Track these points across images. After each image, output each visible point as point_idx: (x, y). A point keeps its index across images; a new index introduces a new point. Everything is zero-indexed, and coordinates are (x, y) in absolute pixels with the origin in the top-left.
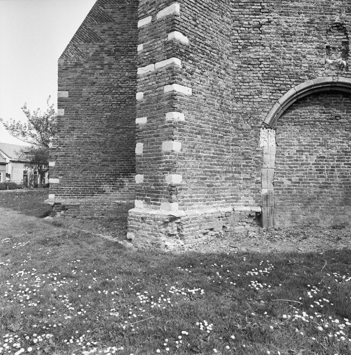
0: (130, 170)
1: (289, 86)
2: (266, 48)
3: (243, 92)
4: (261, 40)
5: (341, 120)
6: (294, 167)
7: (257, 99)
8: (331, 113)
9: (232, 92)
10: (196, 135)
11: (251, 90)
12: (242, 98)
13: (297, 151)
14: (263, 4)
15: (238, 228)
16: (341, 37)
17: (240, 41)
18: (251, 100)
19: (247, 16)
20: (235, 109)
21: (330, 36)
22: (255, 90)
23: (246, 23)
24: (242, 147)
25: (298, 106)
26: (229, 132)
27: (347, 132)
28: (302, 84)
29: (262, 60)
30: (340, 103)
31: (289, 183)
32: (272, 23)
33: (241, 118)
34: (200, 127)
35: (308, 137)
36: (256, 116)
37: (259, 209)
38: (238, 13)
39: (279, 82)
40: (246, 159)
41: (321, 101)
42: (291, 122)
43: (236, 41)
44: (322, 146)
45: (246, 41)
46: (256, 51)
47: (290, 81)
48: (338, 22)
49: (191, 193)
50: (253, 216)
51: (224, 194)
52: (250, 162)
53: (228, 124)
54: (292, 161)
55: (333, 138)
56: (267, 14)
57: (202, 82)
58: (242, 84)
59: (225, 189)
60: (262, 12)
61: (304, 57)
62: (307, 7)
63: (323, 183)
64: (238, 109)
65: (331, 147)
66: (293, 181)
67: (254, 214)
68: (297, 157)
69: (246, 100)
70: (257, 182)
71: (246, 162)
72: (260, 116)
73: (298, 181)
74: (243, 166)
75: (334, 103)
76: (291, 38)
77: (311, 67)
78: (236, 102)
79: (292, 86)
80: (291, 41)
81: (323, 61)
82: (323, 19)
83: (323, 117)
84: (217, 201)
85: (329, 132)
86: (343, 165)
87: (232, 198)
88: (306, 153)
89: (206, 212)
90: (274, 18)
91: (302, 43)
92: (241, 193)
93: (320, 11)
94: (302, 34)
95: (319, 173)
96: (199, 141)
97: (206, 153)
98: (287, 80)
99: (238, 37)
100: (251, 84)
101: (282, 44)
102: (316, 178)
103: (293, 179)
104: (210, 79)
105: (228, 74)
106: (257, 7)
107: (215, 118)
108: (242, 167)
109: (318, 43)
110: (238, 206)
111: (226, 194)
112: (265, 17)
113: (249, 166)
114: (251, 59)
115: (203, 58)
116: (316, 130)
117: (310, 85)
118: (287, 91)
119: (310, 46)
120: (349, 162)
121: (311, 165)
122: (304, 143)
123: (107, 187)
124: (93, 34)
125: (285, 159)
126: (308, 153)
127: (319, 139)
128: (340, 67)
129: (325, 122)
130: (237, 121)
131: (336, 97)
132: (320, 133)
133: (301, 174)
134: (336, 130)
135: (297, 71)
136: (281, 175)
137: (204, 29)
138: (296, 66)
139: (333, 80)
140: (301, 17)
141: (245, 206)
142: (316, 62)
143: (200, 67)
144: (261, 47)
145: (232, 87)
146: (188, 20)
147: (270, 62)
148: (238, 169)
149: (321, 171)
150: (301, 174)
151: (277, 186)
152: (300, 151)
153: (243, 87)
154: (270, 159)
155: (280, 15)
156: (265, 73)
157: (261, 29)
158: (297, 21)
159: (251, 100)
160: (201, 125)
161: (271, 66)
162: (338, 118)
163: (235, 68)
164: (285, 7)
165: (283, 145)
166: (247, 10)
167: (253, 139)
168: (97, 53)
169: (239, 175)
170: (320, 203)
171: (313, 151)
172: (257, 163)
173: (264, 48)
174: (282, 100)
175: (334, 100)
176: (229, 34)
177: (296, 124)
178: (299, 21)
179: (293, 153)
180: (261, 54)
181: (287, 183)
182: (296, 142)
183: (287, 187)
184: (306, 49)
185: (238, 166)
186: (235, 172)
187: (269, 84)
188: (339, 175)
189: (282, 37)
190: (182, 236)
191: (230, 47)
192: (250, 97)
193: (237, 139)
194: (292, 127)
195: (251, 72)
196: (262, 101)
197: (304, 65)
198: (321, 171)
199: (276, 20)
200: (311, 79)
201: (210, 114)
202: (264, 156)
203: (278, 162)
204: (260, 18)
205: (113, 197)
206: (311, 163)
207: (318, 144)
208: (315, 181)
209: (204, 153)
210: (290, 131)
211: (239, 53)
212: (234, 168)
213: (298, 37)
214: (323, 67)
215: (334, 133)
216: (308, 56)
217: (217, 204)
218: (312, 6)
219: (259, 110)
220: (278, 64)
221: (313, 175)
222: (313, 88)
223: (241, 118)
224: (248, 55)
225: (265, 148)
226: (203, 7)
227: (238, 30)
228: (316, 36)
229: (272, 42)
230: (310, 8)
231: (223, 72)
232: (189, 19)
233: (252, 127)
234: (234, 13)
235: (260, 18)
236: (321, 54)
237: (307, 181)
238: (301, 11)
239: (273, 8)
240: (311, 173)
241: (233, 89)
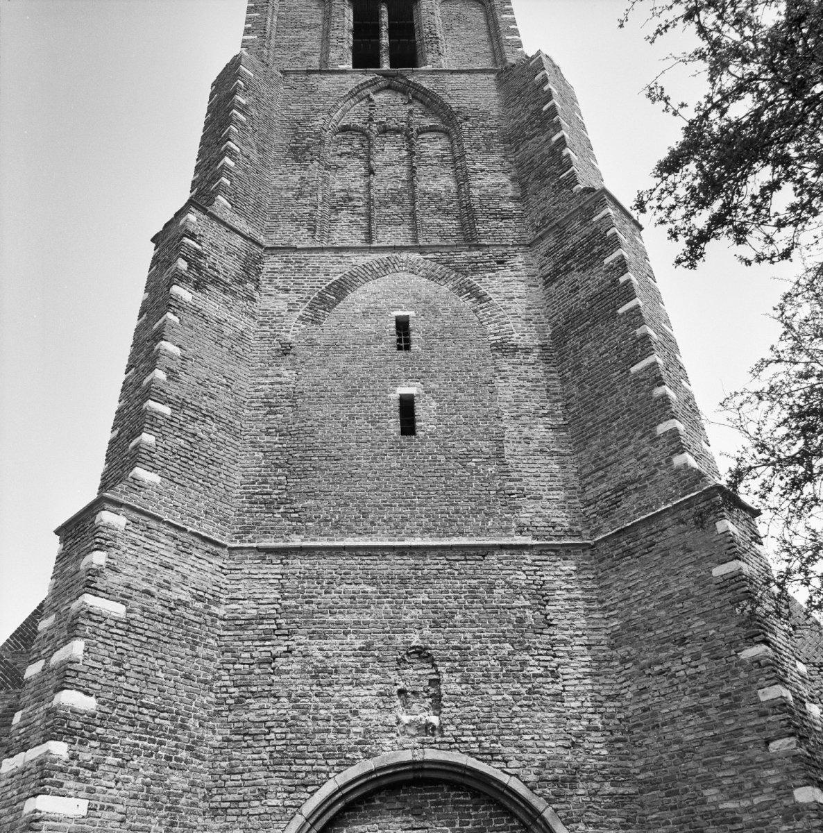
128: (428, 728)
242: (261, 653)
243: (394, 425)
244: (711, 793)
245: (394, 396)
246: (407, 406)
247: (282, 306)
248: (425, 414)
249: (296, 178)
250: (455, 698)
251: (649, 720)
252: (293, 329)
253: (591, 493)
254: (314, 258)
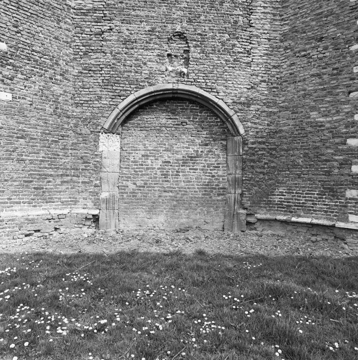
1: (129, 92)
2: (107, 54)
3: (82, 98)
4: (102, 47)
5: (187, 126)
6: (140, 171)
7: (97, 104)
8: (177, 119)
9: (72, 98)
10: (17, 139)
11: (91, 96)
12: (82, 104)
13: (143, 156)
14: (105, 12)
15: (74, 230)
16: (183, 46)
17: (81, 48)
18: (91, 106)
19: (90, 23)
20: (75, 114)
21: (172, 45)
22: (94, 96)
23: (88, 30)
24: (81, 151)
25: (143, 111)
26: (68, 136)
27: (193, 138)
28: (142, 90)
29: (103, 66)
30: (186, 109)
31: (134, 187)
32: (114, 30)
33: (80, 123)
34: (24, 131)
35: (154, 143)
36: (95, 121)
37: (96, 212)
38: (80, 20)
39: (119, 88)
40: (84, 163)
41: (167, 107)
42: (137, 127)
43: (77, 47)
44: (167, 151)
45: (88, 47)
46: (97, 58)
47: (130, 87)
48: (179, 31)
49: (10, 195)
50: (91, 219)
51: (59, 196)
52: (89, 166)
53: (65, 128)
54: (137, 165)
55: (179, 144)
56: (109, 22)
57: (27, 88)
58: (82, 89)
59: (60, 192)
60: (104, 20)
61: (145, 64)
62: (149, 16)
63: (168, 187)
64: (78, 114)
65: (177, 152)
66: (138, 185)
67: (91, 217)
68: (142, 161)
69: (86, 105)
70: (96, 186)
71: (85, 166)
72: (99, 121)
73: (143, 185)
74: (82, 170)
75: (181, 109)
76: (132, 46)
77: (152, 74)
78: (76, 108)
79: (132, 92)
80: (132, 49)
81: (163, 68)
82: (164, 28)
83: (169, 122)
84: (49, 204)
85: (174, 138)
86: (188, 170)
87: (71, 201)
88: (151, 158)
89: (29, 214)
90: (116, 26)
91: (143, 51)
92: (80, 196)
93: (161, 20)
94: (144, 42)
95: (164, 178)
96: (21, 145)
97: (32, 156)
98: (127, 86)
99: (79, 44)
100: (91, 90)
101: (123, 51)
102: (161, 182)
103: (138, 183)
104: (40, 84)
105: (66, 79)
106: (99, 15)
107: (46, 122)
108: (80, 171)
109: (159, 51)
110: (76, 208)
111: (62, 197)
112: (107, 24)
113: (88, 170)
114: (91, 66)
115: (29, 64)
116: (162, 135)
117: (150, 91)
118: (127, 97)
119: (151, 54)
120: (194, 167)
121: (156, 170)
122: (150, 148)
125: (130, 163)
126: (153, 158)
127: (165, 145)
128: (181, 74)
129: (171, 127)
130: (76, 126)
131: (182, 103)
132: (166, 138)
133: (145, 178)
134: (182, 135)
135: (137, 77)
136: (126, 179)
137: (31, 36)
138: (136, 72)
139: (173, 87)
140: (143, 26)
141: (83, 208)
142: (156, 69)
143: (25, 73)
144: (102, 54)
145: (72, 92)
146: (5, 27)
147: (111, 68)
148: (77, 173)
149: (166, 176)
150: (145, 178)
151: (122, 189)
152: (146, 156)
153: (83, 92)
155: (122, 23)
156: (106, 80)
157: (102, 36)
158: (138, 29)
159: (91, 106)
160: (25, 130)
161: (112, 73)
162: (184, 124)
163: (76, 74)
164: (126, 15)
165: (129, 149)
166: (90, 17)
167: (92, 144)
169: (77, 178)
170: (164, 206)
171: (159, 156)
172: (96, 167)
173: (105, 54)
174: (122, 105)
175: (180, 106)
176: (69, 40)
177: (142, 129)
178: (141, 29)
179: (138, 158)
180: (102, 60)
181: (132, 187)
182: (141, 147)
183: (132, 191)
184: (147, 57)
185: (77, 170)
186: (74, 176)
187: (109, 90)
188: (184, 179)
189: (123, 44)
191: (71, 53)
192: (89, 102)
193: (76, 144)
194: (138, 131)
195: (92, 78)
196: (101, 107)
197: (144, 72)
198: (166, 176)
199: (117, 28)
200: (151, 86)
201: (39, 119)
202: (103, 160)
203: (123, 166)
204: (102, 26)
206: (156, 167)
207: (164, 149)
208: (159, 185)
209: (29, 156)
211: (80, 59)
212: (73, 171)
213: (139, 45)
214: (163, 74)
215: (180, 139)
216: (149, 63)
217: (48, 207)
218: (153, 14)
219: (99, 115)
220: (118, 71)
221: (158, 179)
222: (153, 94)
223: (80, 123)
224: (89, 62)
225: (103, 152)
226: (29, 14)
227: (79, 37)
228: (157, 44)
229: (113, 49)
230: (152, 17)
231: (59, 77)
232: (7, 25)
233: (91, 132)
234: (76, 20)
235: (102, 26)
236: (161, 61)
237: (152, 185)
238: (143, 19)
239: (115, 16)
240: (156, 178)
241: (73, 94)
244: (314, 114)
250: (197, 60)
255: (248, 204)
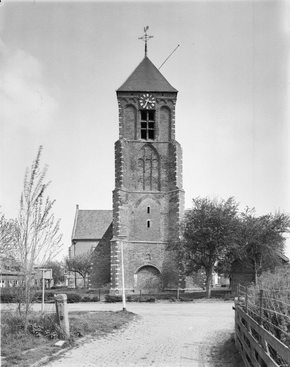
0: (110, 281)
123: (103, 286)
124: (99, 249)
128: (149, 262)
154: (136, 280)
168: (100, 254)
174: (138, 269)
190: (119, 293)
205: (104, 288)
210: (140, 274)
242: (132, 254)
243: (147, 225)
244: (174, 270)
245: (147, 221)
246: (149, 222)
247: (132, 204)
248: (151, 224)
249: (132, 174)
250: (152, 260)
251: (170, 263)
252: (133, 209)
253: (169, 237)
254: (136, 194)
255: (163, 287)
